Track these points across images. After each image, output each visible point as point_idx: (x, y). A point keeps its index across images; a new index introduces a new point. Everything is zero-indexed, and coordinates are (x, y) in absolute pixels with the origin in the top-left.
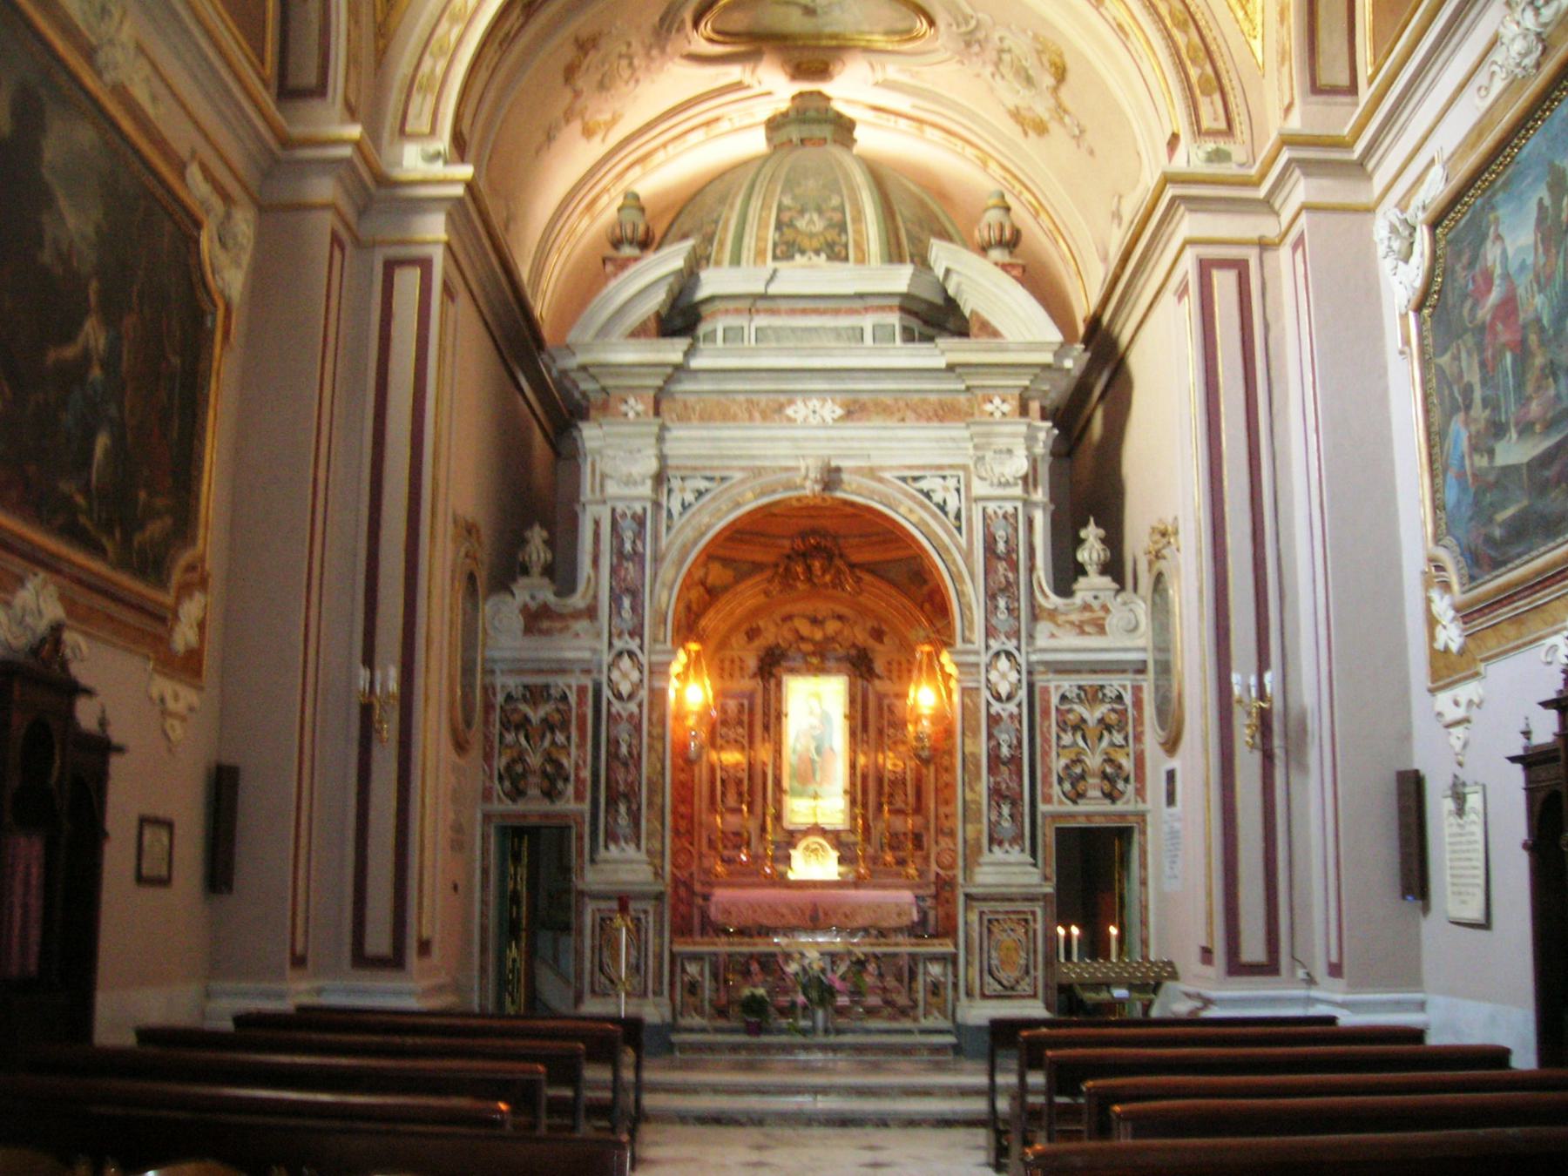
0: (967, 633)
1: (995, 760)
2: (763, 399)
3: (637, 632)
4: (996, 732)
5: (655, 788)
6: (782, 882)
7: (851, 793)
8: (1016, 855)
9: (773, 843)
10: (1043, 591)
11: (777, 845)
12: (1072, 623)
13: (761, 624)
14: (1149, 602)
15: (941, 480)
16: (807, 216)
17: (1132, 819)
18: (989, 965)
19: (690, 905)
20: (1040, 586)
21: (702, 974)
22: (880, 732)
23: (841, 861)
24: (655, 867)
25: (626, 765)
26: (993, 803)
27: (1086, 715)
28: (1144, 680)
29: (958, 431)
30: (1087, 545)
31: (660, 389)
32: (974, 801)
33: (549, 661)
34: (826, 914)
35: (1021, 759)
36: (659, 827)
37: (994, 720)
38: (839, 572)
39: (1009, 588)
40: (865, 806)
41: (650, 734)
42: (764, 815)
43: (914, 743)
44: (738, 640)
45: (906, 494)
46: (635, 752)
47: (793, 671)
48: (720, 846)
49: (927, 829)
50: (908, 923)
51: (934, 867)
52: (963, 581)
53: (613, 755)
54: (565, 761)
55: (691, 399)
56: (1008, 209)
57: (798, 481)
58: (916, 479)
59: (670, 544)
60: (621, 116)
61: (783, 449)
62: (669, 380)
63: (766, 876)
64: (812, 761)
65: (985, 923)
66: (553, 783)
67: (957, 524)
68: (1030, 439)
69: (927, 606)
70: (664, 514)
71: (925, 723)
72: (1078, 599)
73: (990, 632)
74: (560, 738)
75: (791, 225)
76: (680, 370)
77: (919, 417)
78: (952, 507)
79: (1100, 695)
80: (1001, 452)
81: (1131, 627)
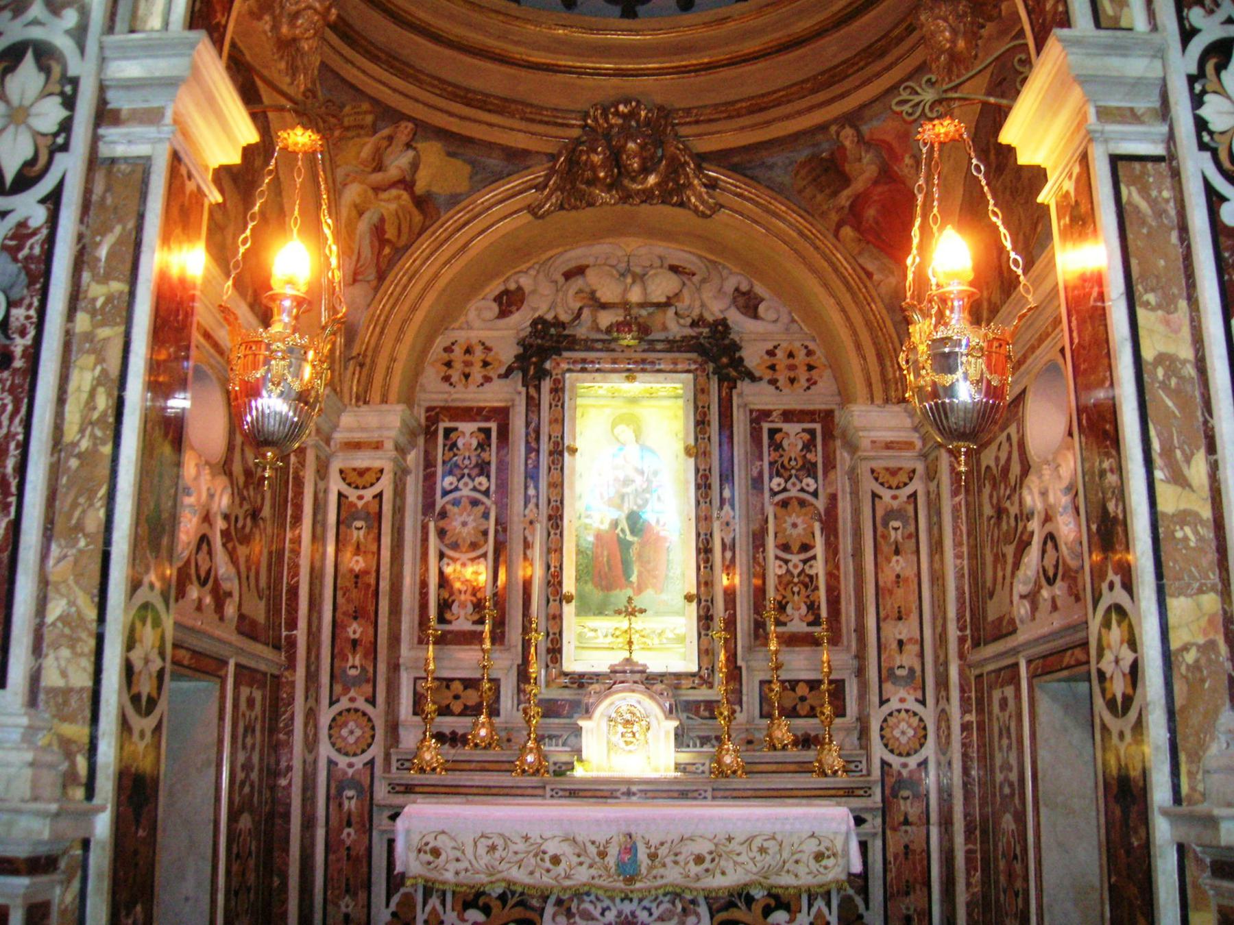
9: (540, 703)
11: (551, 709)
13: (525, 282)
19: (367, 826)
23: (681, 738)
32: (1184, 517)
34: (653, 856)
36: (92, 614)
38: (675, 168)
42: (526, 644)
44: (480, 311)
51: (878, 751)
64: (624, 545)
69: (847, 232)
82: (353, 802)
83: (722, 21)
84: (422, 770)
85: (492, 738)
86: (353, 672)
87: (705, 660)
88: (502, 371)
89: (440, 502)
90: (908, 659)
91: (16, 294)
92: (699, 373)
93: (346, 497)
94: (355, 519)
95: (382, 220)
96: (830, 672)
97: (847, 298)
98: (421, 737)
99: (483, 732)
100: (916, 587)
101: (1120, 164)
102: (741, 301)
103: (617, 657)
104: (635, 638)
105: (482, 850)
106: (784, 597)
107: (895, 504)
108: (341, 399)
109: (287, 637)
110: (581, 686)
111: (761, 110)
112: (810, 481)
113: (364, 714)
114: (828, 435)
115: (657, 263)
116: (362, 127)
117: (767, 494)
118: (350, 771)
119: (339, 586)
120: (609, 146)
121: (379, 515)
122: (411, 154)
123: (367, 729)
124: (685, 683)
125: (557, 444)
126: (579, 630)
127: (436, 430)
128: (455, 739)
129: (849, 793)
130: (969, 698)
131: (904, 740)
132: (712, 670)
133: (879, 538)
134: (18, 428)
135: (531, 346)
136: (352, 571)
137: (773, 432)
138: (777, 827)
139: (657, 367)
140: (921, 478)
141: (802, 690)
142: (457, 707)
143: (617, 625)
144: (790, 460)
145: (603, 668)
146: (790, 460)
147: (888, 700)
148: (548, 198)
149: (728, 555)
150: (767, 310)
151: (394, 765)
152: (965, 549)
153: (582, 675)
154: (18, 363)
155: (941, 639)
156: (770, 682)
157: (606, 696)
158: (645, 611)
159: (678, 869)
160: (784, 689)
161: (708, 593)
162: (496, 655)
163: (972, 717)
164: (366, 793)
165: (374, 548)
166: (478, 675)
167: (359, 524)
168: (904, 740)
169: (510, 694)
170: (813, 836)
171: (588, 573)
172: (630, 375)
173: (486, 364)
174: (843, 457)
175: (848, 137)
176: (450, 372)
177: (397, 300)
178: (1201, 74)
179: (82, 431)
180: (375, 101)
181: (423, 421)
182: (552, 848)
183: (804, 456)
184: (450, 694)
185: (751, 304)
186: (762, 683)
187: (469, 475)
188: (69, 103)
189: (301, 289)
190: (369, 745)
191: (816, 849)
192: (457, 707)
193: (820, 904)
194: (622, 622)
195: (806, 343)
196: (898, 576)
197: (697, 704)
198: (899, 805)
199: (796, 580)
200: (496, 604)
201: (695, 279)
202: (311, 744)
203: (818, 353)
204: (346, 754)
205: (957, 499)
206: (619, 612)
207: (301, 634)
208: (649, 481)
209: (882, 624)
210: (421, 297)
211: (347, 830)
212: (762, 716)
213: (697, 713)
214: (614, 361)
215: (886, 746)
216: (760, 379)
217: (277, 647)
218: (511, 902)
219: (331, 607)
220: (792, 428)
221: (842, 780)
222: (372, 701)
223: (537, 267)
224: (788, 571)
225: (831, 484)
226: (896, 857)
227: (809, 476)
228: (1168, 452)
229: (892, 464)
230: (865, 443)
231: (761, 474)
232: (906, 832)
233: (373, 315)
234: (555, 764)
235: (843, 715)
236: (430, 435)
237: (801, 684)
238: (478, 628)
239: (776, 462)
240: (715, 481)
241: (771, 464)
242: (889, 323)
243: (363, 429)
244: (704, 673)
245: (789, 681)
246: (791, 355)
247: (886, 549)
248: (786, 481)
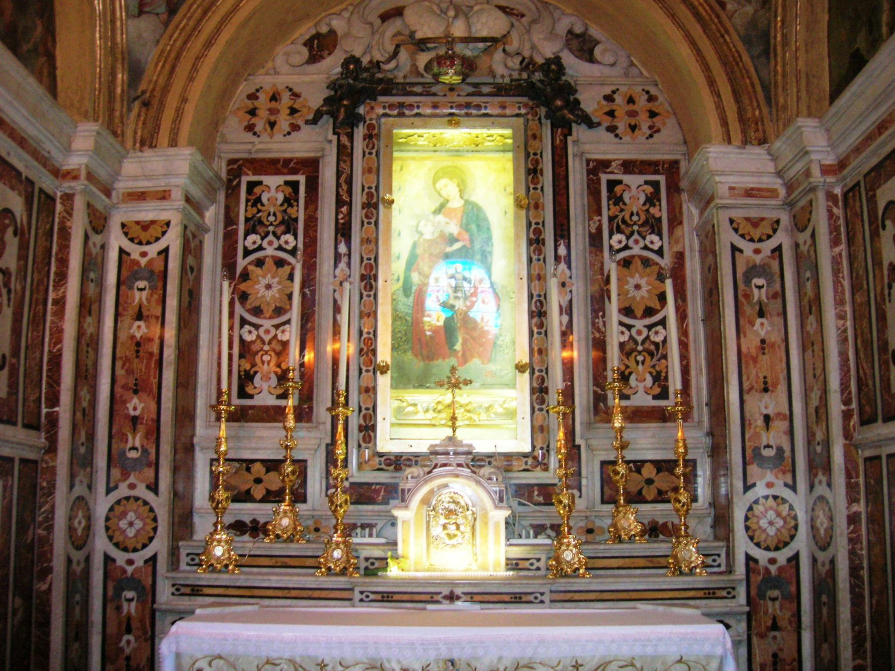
13: (338, 24)
47: (401, 112)
51: (742, 545)
63: (356, 67)
64: (386, 460)
82: (133, 604)
85: (295, 529)
86: (133, 455)
87: (539, 437)
88: (311, 117)
89: (241, 263)
90: (776, 437)
92: (530, 117)
93: (128, 254)
94: (137, 279)
96: (686, 453)
97: (696, 30)
98: (212, 529)
99: (285, 522)
100: (783, 354)
102: (575, 44)
103: (437, 436)
104: (459, 413)
106: (627, 367)
107: (758, 259)
108: (123, 143)
109: (48, 414)
110: (398, 468)
112: (655, 238)
113: (146, 503)
114: (674, 188)
118: (130, 569)
119: (118, 354)
123: (148, 521)
125: (370, 195)
126: (396, 404)
127: (239, 184)
128: (256, 529)
129: (710, 593)
130: (857, 484)
131: (772, 531)
133: (740, 297)
135: (341, 86)
136: (133, 337)
137: (612, 184)
138: (637, 650)
139: (483, 111)
140: (786, 230)
142: (258, 492)
143: (440, 399)
144: (632, 214)
145: (422, 448)
146: (632, 214)
147: (754, 485)
149: (565, 319)
150: (605, 51)
151: (184, 559)
152: (848, 308)
155: (821, 413)
156: (614, 463)
157: (426, 482)
158: (471, 382)
160: (630, 470)
161: (542, 362)
162: (302, 434)
163: (860, 507)
164: (148, 594)
165: (158, 312)
167: (141, 284)
169: (318, 477)
170: (680, 661)
171: (407, 341)
172: (452, 121)
173: (293, 111)
174: (691, 212)
176: (254, 121)
177: (190, 36)
181: (224, 175)
183: (647, 210)
184: (251, 478)
185: (586, 48)
186: (604, 464)
187: (274, 234)
190: (151, 539)
192: (258, 492)
194: (446, 396)
195: (647, 88)
196: (763, 341)
197: (530, 487)
198: (766, 606)
199: (640, 348)
200: (302, 376)
201: (524, 20)
203: (661, 99)
204: (125, 549)
205: (837, 250)
206: (440, 385)
207: (64, 409)
208: (476, 288)
209: (746, 397)
210: (218, 31)
211: (126, 638)
212: (603, 502)
213: (530, 498)
214: (435, 106)
215: (751, 538)
216: (599, 124)
217: (32, 425)
219: (109, 380)
220: (634, 181)
221: (701, 579)
223: (351, 8)
224: (631, 337)
225: (677, 242)
227: (652, 232)
229: (754, 214)
230: (723, 190)
231: (599, 229)
232: (775, 638)
233: (162, 51)
234: (367, 559)
236: (232, 190)
237: (647, 465)
238: (281, 403)
239: (617, 216)
241: (611, 219)
242: (746, 58)
243: (147, 177)
245: (634, 462)
246: (631, 100)
247: (749, 311)
248: (628, 238)
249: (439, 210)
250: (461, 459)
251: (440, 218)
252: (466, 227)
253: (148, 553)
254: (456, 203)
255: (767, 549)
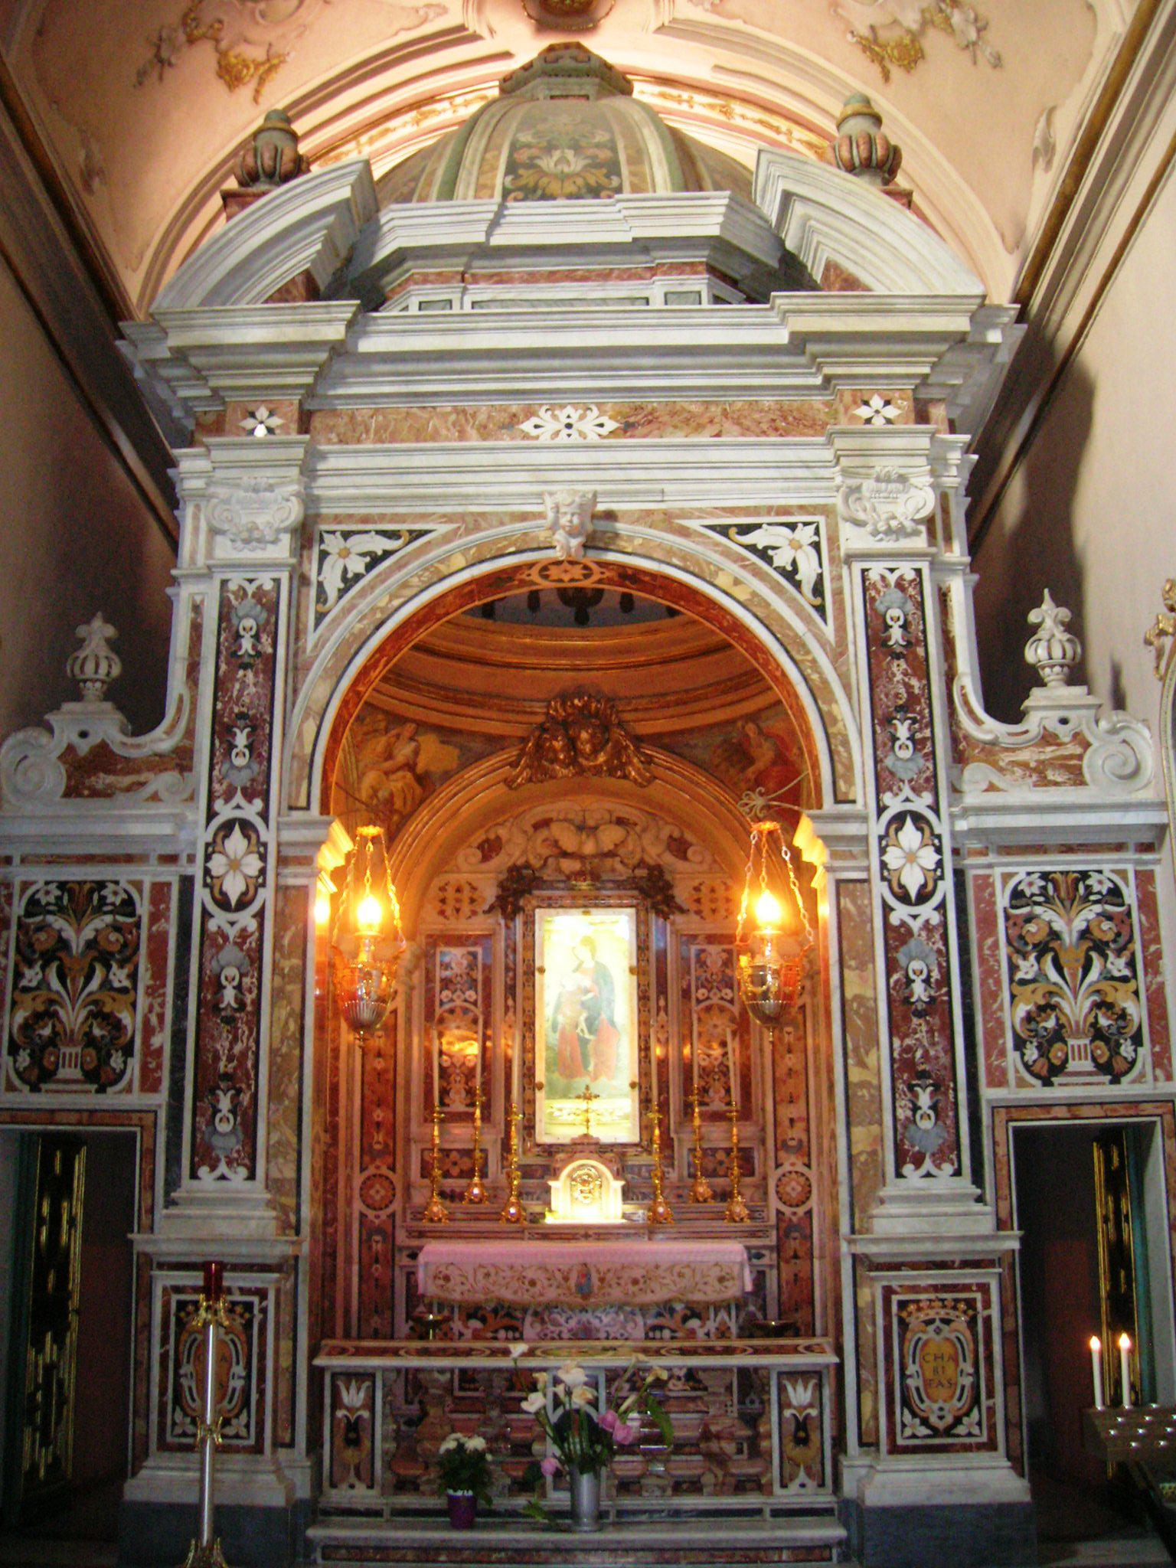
0: (842, 786)
1: (901, 1007)
2: (484, 405)
3: (258, 790)
4: (901, 957)
5: (286, 1067)
6: (534, 1228)
7: (641, 1085)
8: (944, 1181)
9: (520, 1167)
10: (971, 712)
11: (527, 1172)
12: (1024, 765)
13: (502, 832)
14: (1155, 729)
15: (785, 531)
16: (557, 155)
17: (1149, 1108)
18: (905, 1389)
19: (391, 1263)
20: (964, 696)
21: (370, 1405)
22: (686, 994)
23: (627, 1194)
24: (284, 1209)
25: (230, 1021)
26: (901, 1086)
27: (1059, 925)
28: (1158, 862)
29: (814, 451)
30: (1042, 634)
31: (310, 391)
32: (863, 1084)
33: (102, 838)
34: (602, 1280)
35: (950, 1002)
36: (294, 1140)
37: (897, 936)
38: (618, 750)
39: (912, 706)
40: (664, 1107)
41: (276, 968)
42: (508, 1124)
43: (750, 988)
44: (468, 856)
45: (727, 553)
46: (249, 998)
47: (550, 904)
48: (437, 1172)
49: (763, 1142)
50: (738, 1294)
51: (774, 1203)
52: (831, 699)
53: (210, 1007)
54: (125, 1018)
55: (364, 409)
56: (877, 120)
57: (543, 536)
58: (745, 529)
59: (319, 645)
60: (282, 59)
61: (517, 484)
62: (322, 373)
64: (584, 1042)
65: (894, 1308)
66: (104, 1059)
67: (818, 601)
68: (937, 463)
70: (313, 592)
71: (768, 950)
72: (1033, 723)
73: (883, 781)
74: (119, 977)
75: (531, 165)
76: (338, 350)
77: (746, 431)
78: (807, 573)
79: (1081, 890)
80: (888, 480)
81: (1129, 770)
83: (656, 631)
84: (431, 1220)
88: (486, 907)
89: (438, 1011)
91: (243, 970)
95: (392, 795)
101: (842, 885)
103: (576, 1132)
104: (591, 1116)
105: (480, 1277)
111: (685, 703)
112: (728, 991)
115: (607, 816)
116: (376, 731)
117: (694, 1002)
118: (377, 1222)
120: (566, 736)
121: (395, 1027)
122: (413, 744)
124: (631, 1151)
131: (794, 1194)
132: (651, 1141)
134: (252, 1044)
136: (375, 1069)
138: (692, 1258)
141: (721, 1156)
142: (455, 1171)
148: (521, 773)
150: (695, 852)
151: (409, 1216)
153: (551, 1146)
154: (249, 1008)
159: (619, 1289)
164: (389, 1237)
166: (470, 1146)
168: (794, 1194)
173: (472, 901)
175: (751, 729)
178: (887, 834)
179: (282, 1042)
180: (386, 712)
182: (530, 1274)
188: (263, 857)
189: (374, 932)
191: (718, 1274)
192: (455, 1171)
193: (723, 1315)
194: (582, 1104)
201: (638, 829)
202: (349, 1202)
206: (578, 1097)
218: (502, 1313)
222: (393, 1168)
226: (787, 1283)
228: (856, 1049)
231: (689, 986)
235: (752, 1174)
238: (471, 1110)
240: (653, 993)
241: (697, 979)
244: (645, 1143)
249: (578, 969)
250: (592, 1148)
251: (578, 975)
252: (596, 982)
253: (390, 1210)
254: (589, 964)
255: (791, 1206)
